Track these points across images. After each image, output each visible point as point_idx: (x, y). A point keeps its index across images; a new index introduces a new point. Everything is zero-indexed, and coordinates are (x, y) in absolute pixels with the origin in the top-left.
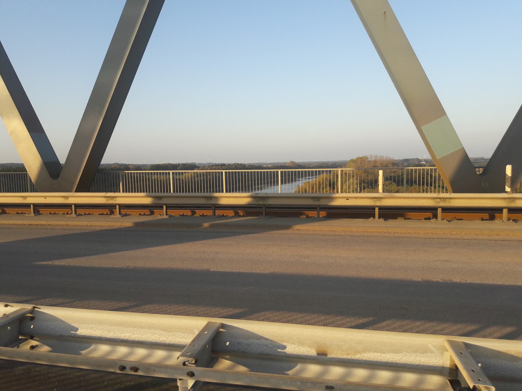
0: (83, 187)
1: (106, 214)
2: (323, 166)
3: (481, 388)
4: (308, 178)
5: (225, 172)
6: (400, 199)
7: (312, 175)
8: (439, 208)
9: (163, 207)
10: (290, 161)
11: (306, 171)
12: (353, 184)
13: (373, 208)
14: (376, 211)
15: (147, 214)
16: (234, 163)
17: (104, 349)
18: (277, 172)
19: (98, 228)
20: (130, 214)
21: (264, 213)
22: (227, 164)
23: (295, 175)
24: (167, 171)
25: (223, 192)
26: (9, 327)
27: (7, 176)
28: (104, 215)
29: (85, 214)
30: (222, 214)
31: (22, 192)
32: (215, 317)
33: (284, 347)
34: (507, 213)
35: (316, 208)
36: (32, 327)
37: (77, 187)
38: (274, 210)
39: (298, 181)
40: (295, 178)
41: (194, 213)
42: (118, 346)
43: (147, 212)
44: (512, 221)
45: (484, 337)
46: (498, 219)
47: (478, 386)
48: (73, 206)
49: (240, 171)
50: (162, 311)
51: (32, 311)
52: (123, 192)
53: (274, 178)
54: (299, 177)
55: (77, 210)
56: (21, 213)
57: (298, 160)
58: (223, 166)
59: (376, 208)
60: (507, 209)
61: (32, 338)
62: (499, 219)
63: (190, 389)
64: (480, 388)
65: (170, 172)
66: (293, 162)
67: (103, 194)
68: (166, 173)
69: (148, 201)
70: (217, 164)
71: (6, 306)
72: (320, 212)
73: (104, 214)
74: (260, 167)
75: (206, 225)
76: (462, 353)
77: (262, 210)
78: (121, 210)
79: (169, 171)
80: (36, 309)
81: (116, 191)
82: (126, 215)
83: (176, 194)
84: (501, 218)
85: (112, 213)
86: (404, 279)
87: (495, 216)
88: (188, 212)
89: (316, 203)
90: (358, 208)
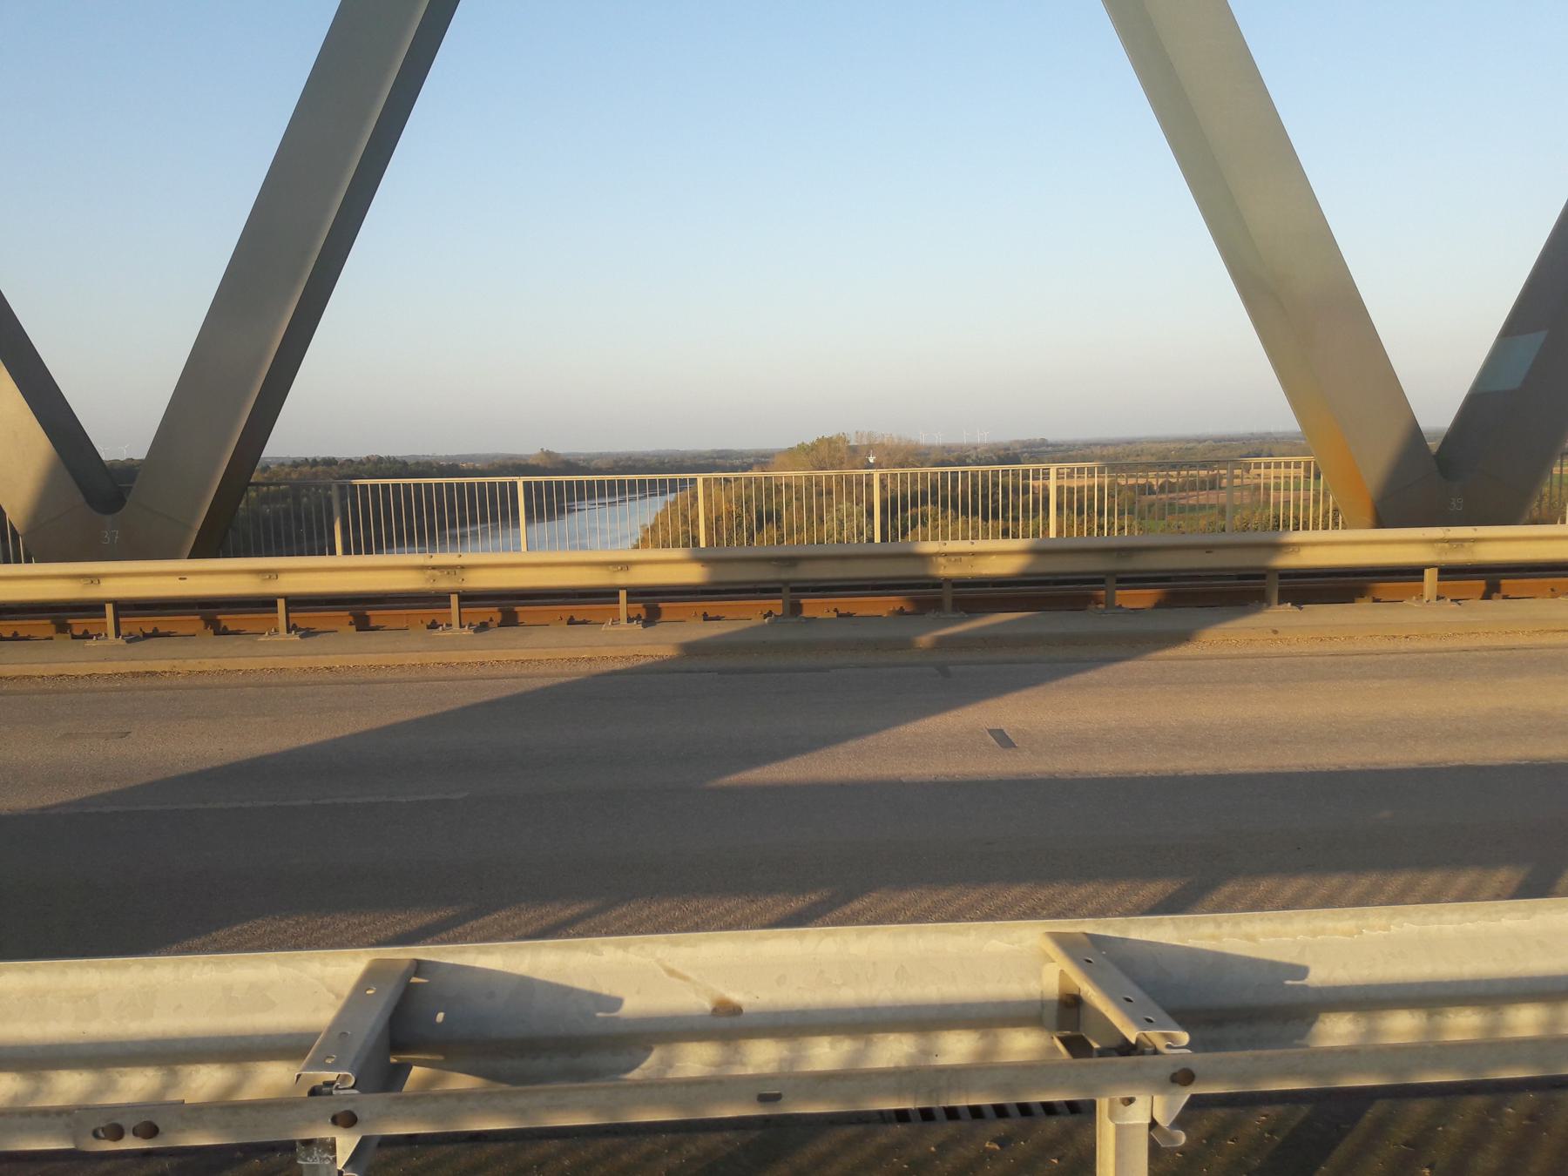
0: (212, 543)
2: (634, 467)
3: (1153, 1040)
7: (612, 494)
9: (618, 594)
11: (580, 483)
12: (850, 515)
15: (715, 616)
16: (365, 456)
17: (696, 1060)
21: (948, 602)
22: (413, 462)
23: (560, 493)
24: (507, 479)
32: (322, 944)
33: (617, 1002)
35: (1102, 581)
37: (197, 537)
38: (1068, 589)
40: (560, 501)
41: (796, 609)
42: (250, 1061)
47: (1144, 1034)
50: (630, 927)
52: (346, 551)
53: (504, 502)
54: (570, 499)
56: (10, 636)
57: (565, 446)
59: (621, 592)
60: (1436, 570)
63: (344, 1167)
64: (1150, 1041)
65: (516, 483)
66: (548, 454)
67: (419, 559)
70: (310, 460)
72: (1118, 592)
73: (21, 635)
74: (452, 469)
76: (1090, 962)
77: (1264, 584)
78: (121, 620)
83: (891, 547)
87: (659, 610)
89: (787, 574)
90: (417, 598)
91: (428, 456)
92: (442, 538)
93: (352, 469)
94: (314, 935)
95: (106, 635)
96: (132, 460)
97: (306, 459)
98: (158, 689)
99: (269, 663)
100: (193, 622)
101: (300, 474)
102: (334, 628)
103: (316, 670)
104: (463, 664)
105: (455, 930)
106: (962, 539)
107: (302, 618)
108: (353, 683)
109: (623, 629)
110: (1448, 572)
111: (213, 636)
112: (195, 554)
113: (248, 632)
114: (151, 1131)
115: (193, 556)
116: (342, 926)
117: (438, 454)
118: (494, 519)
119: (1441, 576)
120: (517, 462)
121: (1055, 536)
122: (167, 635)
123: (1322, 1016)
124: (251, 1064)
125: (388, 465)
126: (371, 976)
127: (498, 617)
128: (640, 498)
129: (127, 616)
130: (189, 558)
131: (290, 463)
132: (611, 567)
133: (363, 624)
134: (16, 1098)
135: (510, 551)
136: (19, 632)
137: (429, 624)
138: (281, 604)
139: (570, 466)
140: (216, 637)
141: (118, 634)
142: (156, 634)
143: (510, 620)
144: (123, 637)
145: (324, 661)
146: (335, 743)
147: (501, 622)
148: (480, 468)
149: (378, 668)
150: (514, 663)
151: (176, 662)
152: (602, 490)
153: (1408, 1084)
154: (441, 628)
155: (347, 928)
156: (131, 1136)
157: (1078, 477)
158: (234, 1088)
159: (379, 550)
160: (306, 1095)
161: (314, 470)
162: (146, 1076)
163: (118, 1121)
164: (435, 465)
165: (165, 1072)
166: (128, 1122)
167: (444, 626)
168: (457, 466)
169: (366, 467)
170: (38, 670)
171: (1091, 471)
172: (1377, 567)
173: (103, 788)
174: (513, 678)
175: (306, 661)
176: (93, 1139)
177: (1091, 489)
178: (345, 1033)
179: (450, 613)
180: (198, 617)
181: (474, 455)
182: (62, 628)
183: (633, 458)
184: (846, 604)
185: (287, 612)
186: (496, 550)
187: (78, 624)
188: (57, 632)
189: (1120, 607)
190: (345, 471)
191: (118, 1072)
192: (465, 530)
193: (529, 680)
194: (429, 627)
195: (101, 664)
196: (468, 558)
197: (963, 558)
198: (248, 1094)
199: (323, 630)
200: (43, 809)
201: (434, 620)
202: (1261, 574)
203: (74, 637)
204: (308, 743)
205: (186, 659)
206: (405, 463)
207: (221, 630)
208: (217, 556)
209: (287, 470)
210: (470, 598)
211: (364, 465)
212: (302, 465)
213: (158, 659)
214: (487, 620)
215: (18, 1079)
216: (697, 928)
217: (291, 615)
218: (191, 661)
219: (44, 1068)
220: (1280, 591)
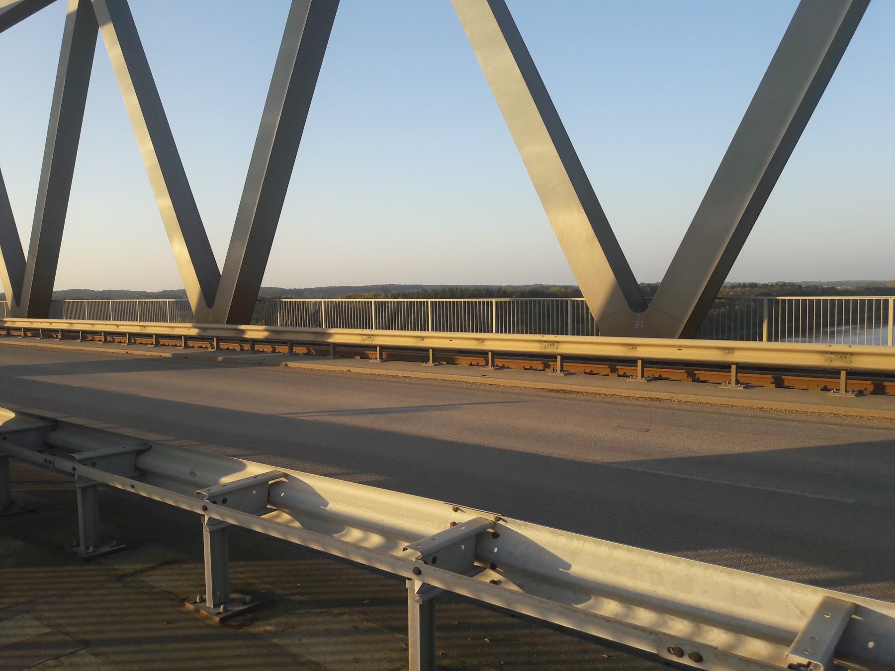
1: (589, 372)
5: (374, 301)
6: (798, 353)
8: (295, 343)
13: (426, 350)
14: (841, 376)
15: (262, 350)
16: (775, 282)
17: (610, 608)
22: (805, 286)
24: (425, 300)
25: (762, 341)
26: (254, 492)
27: (379, 304)
28: (473, 365)
29: (165, 345)
30: (659, 375)
31: (576, 334)
33: (568, 566)
36: (496, 550)
45: (850, 592)
48: (490, 354)
49: (126, 300)
51: (494, 525)
55: (495, 360)
58: (489, 292)
61: (493, 567)
65: (888, 300)
68: (487, 302)
69: (194, 332)
70: (742, 284)
71: (456, 510)
73: (480, 364)
74: (831, 290)
75: (220, 359)
78: (564, 364)
80: (501, 522)
81: (551, 332)
82: (503, 367)
85: (547, 366)
90: (676, 363)
91: (816, 282)
92: (825, 333)
93: (767, 290)
94: (758, 566)
95: (636, 376)
96: (643, 283)
97: (739, 284)
98: (664, 408)
99: (725, 401)
100: (681, 374)
101: (735, 292)
102: (761, 384)
103: (752, 408)
104: (848, 416)
105: (850, 586)
106: (866, 344)
107: (744, 377)
108: (776, 419)
111: (691, 382)
112: (683, 336)
113: (711, 382)
114: (698, 658)
115: (681, 337)
116: (775, 565)
117: (822, 281)
118: (855, 323)
120: (877, 286)
122: (666, 379)
123: (347, 528)
124: (743, 636)
125: (789, 287)
126: (826, 606)
127: (871, 388)
129: (498, 358)
130: (679, 338)
131: (730, 286)
133: (779, 384)
134: (617, 614)
135: (864, 344)
137: (822, 387)
138: (734, 367)
140: (448, 365)
141: (642, 376)
142: (660, 378)
143: (879, 390)
144: (645, 378)
145: (757, 404)
146: (766, 453)
147: (873, 391)
148: (851, 290)
149: (791, 412)
150: (884, 419)
151: (673, 395)
153: (551, 623)
154: (832, 391)
155: (778, 567)
156: (688, 657)
158: (733, 647)
159: (776, 340)
160: (786, 667)
161: (744, 289)
162: (683, 624)
163: (682, 647)
164: (819, 287)
165: (694, 625)
166: (687, 649)
167: (835, 390)
168: (835, 288)
169: (775, 289)
170: (603, 391)
172: (684, 361)
173: (637, 458)
174: (885, 429)
175: (747, 403)
176: (667, 651)
178: (813, 638)
180: (684, 371)
181: (847, 282)
182: (614, 370)
185: (847, 379)
186: (861, 343)
187: (622, 369)
188: (611, 372)
189: (279, 352)
190: (763, 291)
191: (669, 618)
192: (845, 328)
194: (822, 390)
195: (633, 391)
196: (855, 349)
198: (366, 545)
200: (608, 463)
201: (826, 386)
203: (619, 376)
204: (749, 451)
205: (679, 393)
206: (800, 287)
207: (696, 379)
208: (694, 338)
209: (728, 290)
210: (853, 374)
211: (774, 287)
212: (736, 287)
213: (662, 391)
214: (863, 389)
215: (619, 605)
216: (754, 571)
217: (739, 374)
218: (682, 395)
219: (632, 604)
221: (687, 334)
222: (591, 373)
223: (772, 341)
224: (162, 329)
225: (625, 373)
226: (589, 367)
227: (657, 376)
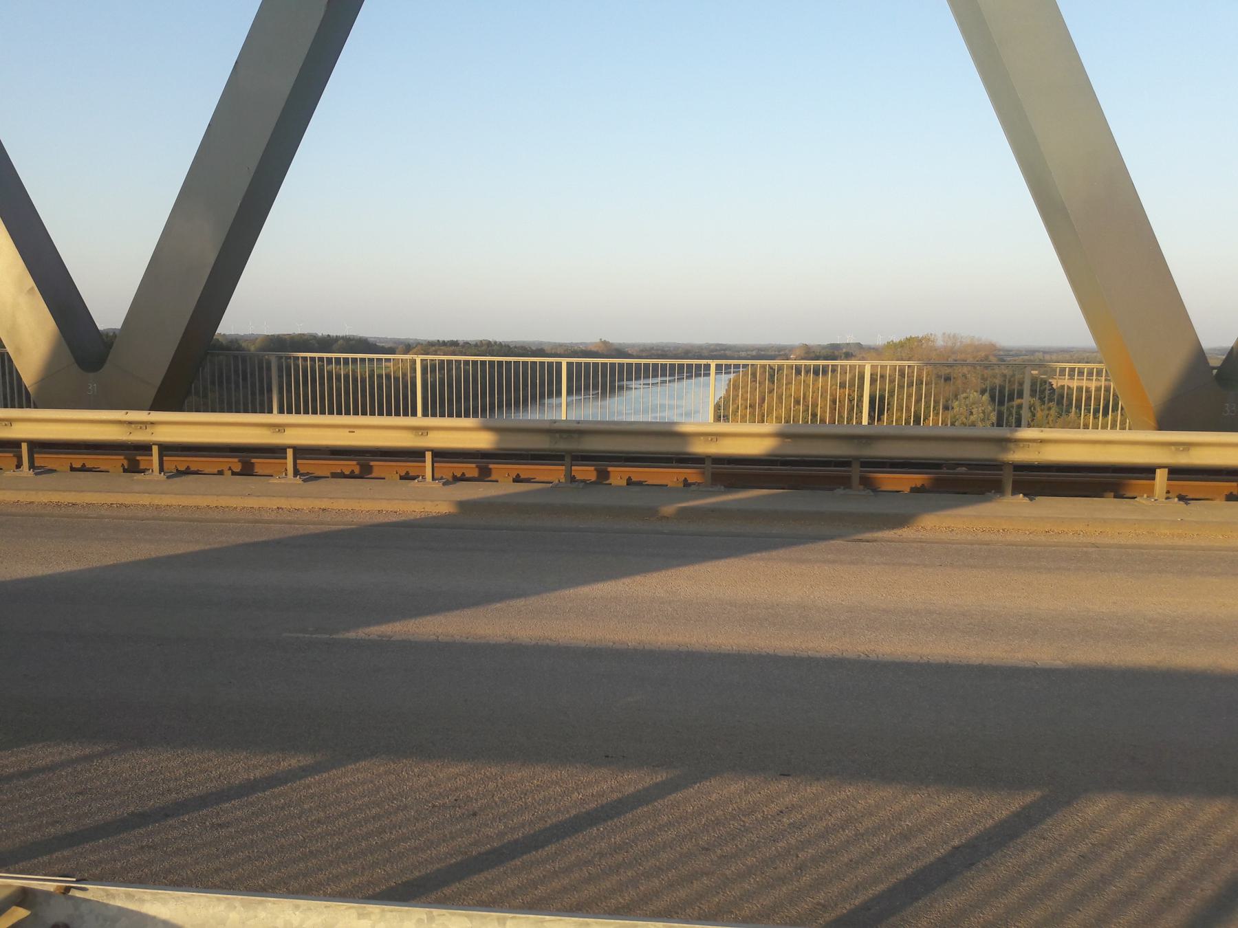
4: (652, 384)
7: (672, 374)
10: (598, 341)
18: (559, 364)
19: (368, 520)
20: (52, 471)
23: (621, 372)
25: (272, 413)
30: (405, 472)
31: (9, 405)
34: (1166, 479)
39: (635, 388)
40: (612, 381)
41: (603, 475)
43: (471, 469)
44: (1176, 499)
46: (1143, 496)
48: (24, 446)
54: (621, 379)
55: (35, 456)
59: (23, 444)
60: (1166, 470)
62: (1145, 496)
65: (415, 360)
66: (605, 343)
69: (482, 440)
70: (498, 343)
74: (540, 352)
77: (1001, 475)
78: (165, 458)
79: (709, 361)
84: (1150, 492)
86: (1209, 672)
88: (586, 472)
89: (562, 445)
97: (438, 341)
102: (382, 476)
109: (429, 486)
110: (1176, 472)
119: (1171, 476)
121: (867, 424)
122: (90, 470)
128: (670, 381)
132: (1173, 448)
136: (410, 472)
139: (620, 352)
141: (161, 470)
142: (188, 472)
143: (247, 470)
152: (655, 371)
157: (1078, 379)
171: (1099, 373)
177: (1098, 389)
179: (286, 463)
183: (655, 348)
184: (638, 473)
193: (1014, 547)
194: (402, 478)
197: (1031, 444)
199: (1203, 498)
202: (998, 466)
217: (435, 465)
220: (1014, 482)
221: (159, 404)
222: (83, 469)
223: (342, 414)
224: (329, 432)
225: (84, 465)
226: (78, 460)
227: (182, 468)
